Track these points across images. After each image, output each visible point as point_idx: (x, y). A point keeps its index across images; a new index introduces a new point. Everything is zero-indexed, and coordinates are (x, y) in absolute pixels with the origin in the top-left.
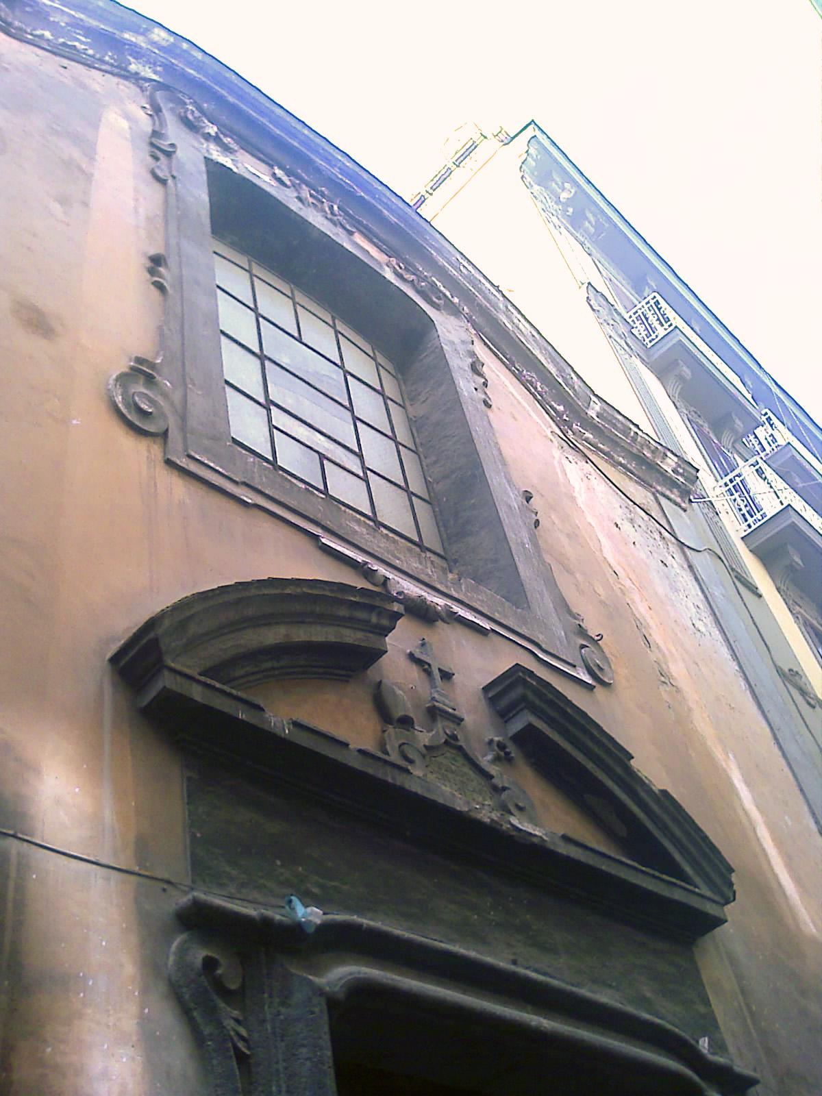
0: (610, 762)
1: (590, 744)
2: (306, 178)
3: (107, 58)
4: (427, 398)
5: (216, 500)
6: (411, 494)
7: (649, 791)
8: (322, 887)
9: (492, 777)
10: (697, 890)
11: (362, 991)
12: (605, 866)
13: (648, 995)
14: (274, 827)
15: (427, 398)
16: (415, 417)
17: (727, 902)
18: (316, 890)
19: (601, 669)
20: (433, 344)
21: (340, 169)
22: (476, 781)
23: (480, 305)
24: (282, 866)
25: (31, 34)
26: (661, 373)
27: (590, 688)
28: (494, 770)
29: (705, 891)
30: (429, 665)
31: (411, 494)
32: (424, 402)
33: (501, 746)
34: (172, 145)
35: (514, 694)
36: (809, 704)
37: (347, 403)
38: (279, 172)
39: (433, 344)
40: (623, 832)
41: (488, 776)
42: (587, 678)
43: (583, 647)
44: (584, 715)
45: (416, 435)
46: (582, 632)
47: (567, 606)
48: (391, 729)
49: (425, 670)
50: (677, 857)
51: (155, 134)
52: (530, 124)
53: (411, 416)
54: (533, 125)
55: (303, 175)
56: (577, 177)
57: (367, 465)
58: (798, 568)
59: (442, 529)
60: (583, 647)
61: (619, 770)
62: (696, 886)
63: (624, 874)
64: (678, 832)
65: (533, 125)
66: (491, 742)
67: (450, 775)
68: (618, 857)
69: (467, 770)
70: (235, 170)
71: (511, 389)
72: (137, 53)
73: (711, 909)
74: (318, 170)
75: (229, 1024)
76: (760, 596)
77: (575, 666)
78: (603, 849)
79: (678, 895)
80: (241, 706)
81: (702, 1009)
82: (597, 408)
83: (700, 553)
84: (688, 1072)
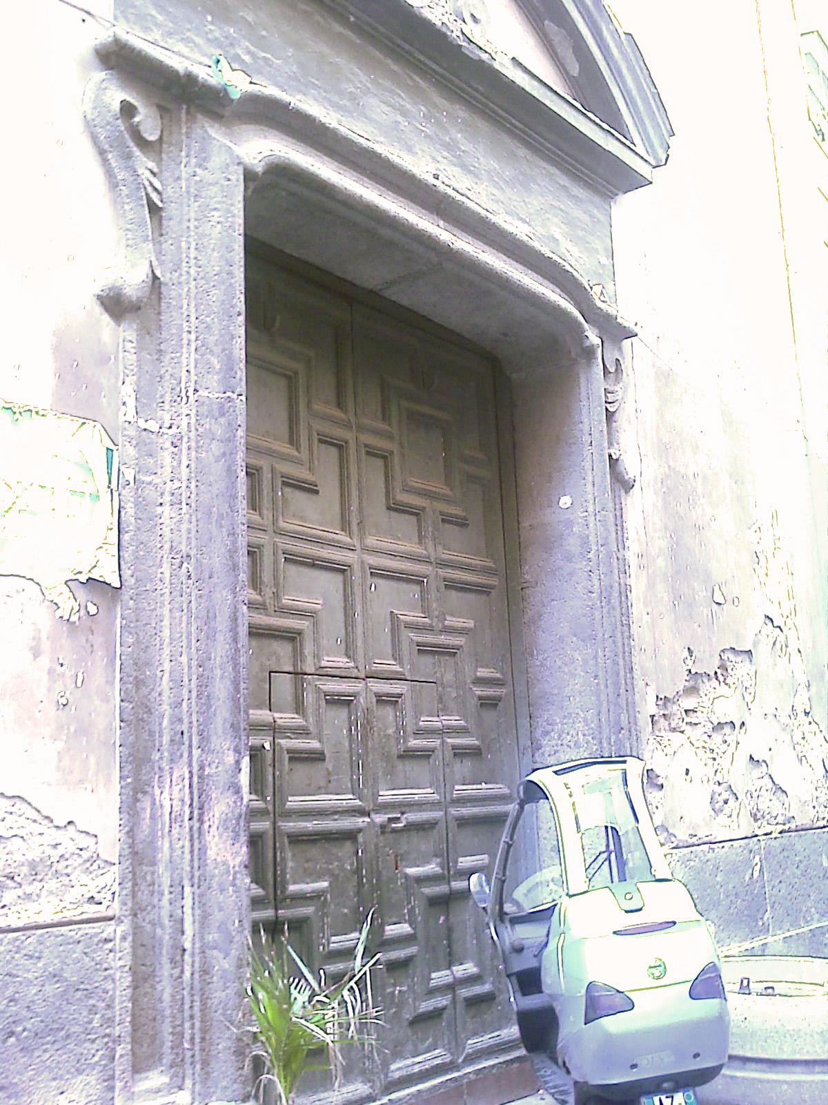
24: (212, 23)
40: (575, 70)
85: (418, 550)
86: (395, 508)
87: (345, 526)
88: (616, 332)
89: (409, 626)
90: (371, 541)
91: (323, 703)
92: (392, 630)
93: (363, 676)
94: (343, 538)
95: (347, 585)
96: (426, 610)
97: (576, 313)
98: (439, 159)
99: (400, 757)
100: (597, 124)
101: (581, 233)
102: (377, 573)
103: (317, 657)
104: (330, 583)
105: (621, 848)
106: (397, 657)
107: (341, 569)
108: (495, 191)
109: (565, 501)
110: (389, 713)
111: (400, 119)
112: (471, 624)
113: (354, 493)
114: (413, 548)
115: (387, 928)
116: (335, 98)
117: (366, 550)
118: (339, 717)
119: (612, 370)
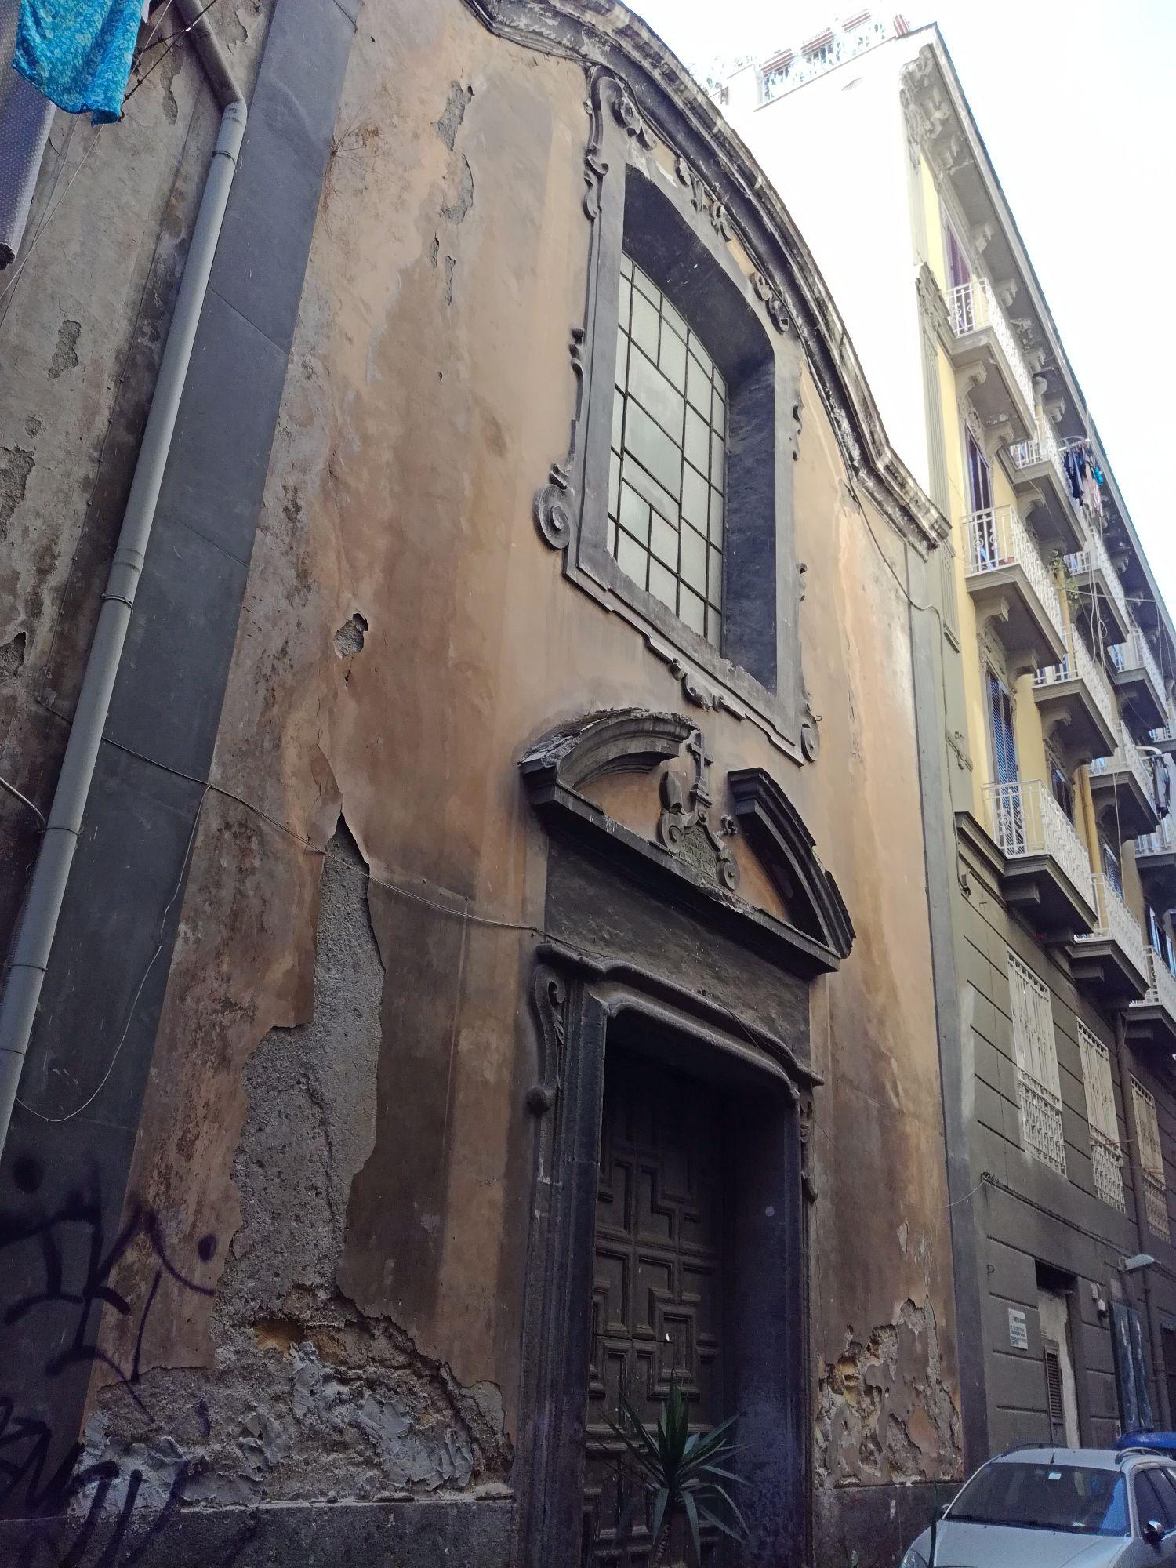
0: (798, 845)
1: (790, 831)
2: (705, 170)
3: (565, 42)
4: (747, 437)
5: (590, 607)
6: (709, 543)
7: (818, 870)
8: (609, 933)
9: (719, 850)
10: (826, 948)
11: (628, 1014)
12: (775, 929)
13: (774, 1016)
14: (591, 891)
15: (747, 437)
16: (730, 452)
17: (844, 956)
18: (607, 936)
19: (812, 747)
20: (769, 380)
21: (738, 166)
22: (709, 853)
23: (819, 332)
24: (592, 919)
25: (509, 26)
26: (958, 363)
27: (799, 765)
28: (721, 844)
29: (832, 949)
30: (699, 755)
31: (709, 543)
32: (742, 439)
33: (730, 824)
34: (605, 167)
35: (749, 787)
36: (960, 765)
37: (680, 445)
38: (683, 164)
39: (769, 380)
40: (790, 894)
41: (716, 849)
42: (800, 758)
43: (805, 725)
44: (792, 809)
45: (727, 472)
46: (807, 711)
47: (803, 686)
48: (667, 815)
49: (695, 759)
50: (825, 931)
51: (592, 151)
52: (927, 27)
53: (727, 451)
54: (932, 30)
55: (703, 167)
56: (958, 102)
57: (683, 515)
58: (1002, 619)
59: (725, 582)
60: (805, 725)
61: (803, 852)
62: (827, 945)
63: (788, 937)
64: (827, 902)
65: (932, 30)
66: (723, 821)
67: (694, 848)
68: (784, 922)
69: (706, 845)
70: (647, 175)
71: (820, 432)
72: (592, 32)
73: (831, 961)
74: (718, 164)
75: (556, 1024)
76: (957, 651)
77: (794, 745)
78: (781, 919)
79: (813, 951)
80: (592, 811)
81: (803, 1028)
82: (887, 461)
83: (922, 612)
84: (786, 1077)
85: (670, 1242)
86: (656, 1209)
87: (627, 1226)
88: (807, 1082)
89: (665, 1301)
90: (644, 1235)
91: (606, 1357)
92: (649, 1302)
93: (630, 1336)
94: (624, 1234)
95: (625, 1268)
96: (670, 1288)
97: (786, 1077)
98: (705, 976)
99: (649, 1399)
100: (802, 936)
101: (788, 1010)
102: (644, 1260)
103: (605, 1323)
104: (616, 1266)
105: (1083, 532)
106: (651, 1323)
107: (622, 1258)
108: (737, 992)
109: (770, 1211)
110: (644, 1365)
111: (684, 954)
112: (935, 1565)
113: (633, 1202)
114: (665, 1239)
115: (634, 1528)
116: (649, 949)
117: (639, 1243)
118: (614, 1367)
119: (805, 1111)
